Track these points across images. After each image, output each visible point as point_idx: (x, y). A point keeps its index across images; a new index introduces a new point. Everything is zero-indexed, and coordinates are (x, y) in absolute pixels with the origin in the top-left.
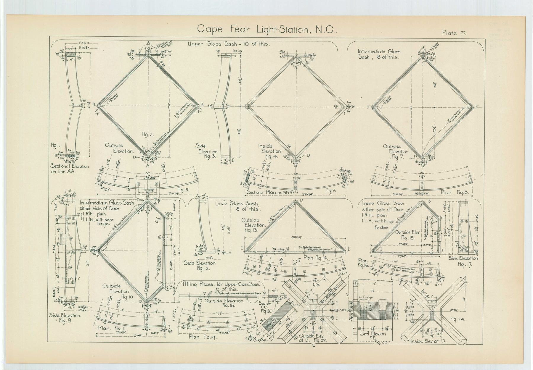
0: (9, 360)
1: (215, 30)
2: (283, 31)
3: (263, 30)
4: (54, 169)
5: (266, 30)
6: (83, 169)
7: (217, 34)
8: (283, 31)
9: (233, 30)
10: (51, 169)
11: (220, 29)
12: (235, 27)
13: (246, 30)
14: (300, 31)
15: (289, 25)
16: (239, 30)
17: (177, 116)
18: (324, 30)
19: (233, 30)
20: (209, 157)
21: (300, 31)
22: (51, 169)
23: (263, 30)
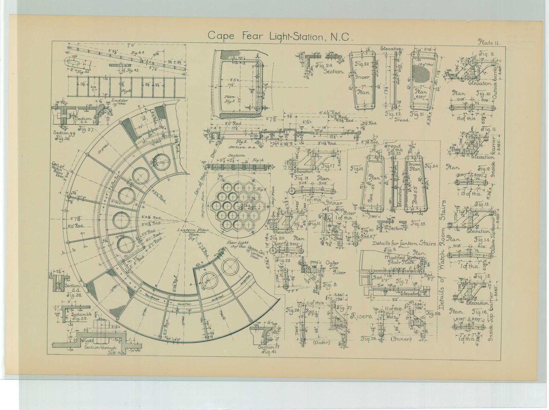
1: (226, 37)
2: (297, 38)
3: (276, 37)
5: (279, 37)
7: (228, 40)
8: (297, 38)
9: (245, 36)
11: (231, 36)
12: (247, 34)
14: (315, 38)
16: (252, 37)
18: (339, 38)
19: (245, 36)
23: (276, 37)
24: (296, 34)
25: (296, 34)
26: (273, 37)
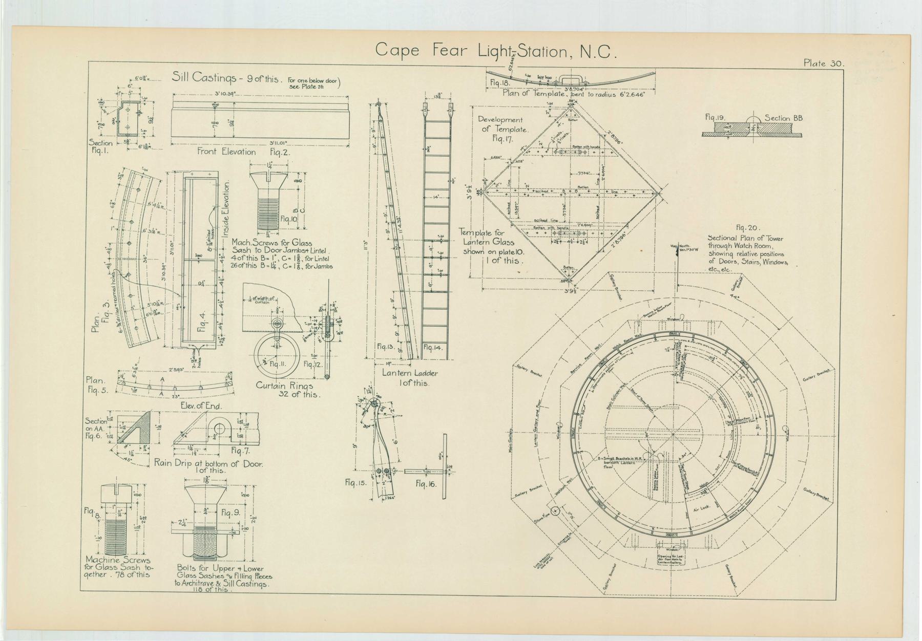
0: (12, 625)
1: (405, 51)
3: (490, 53)
4: (90, 425)
5: (494, 52)
6: (545, 519)
7: (409, 59)
8: (523, 53)
9: (438, 51)
10: (85, 426)
11: (414, 51)
12: (440, 47)
13: (459, 51)
14: (554, 53)
15: (531, 44)
17: (197, 364)
18: (594, 52)
19: (438, 51)
20: (307, 391)
21: (554, 53)
22: (85, 426)
23: (490, 53)
24: (522, 46)
25: (522, 46)
26: (484, 51)
